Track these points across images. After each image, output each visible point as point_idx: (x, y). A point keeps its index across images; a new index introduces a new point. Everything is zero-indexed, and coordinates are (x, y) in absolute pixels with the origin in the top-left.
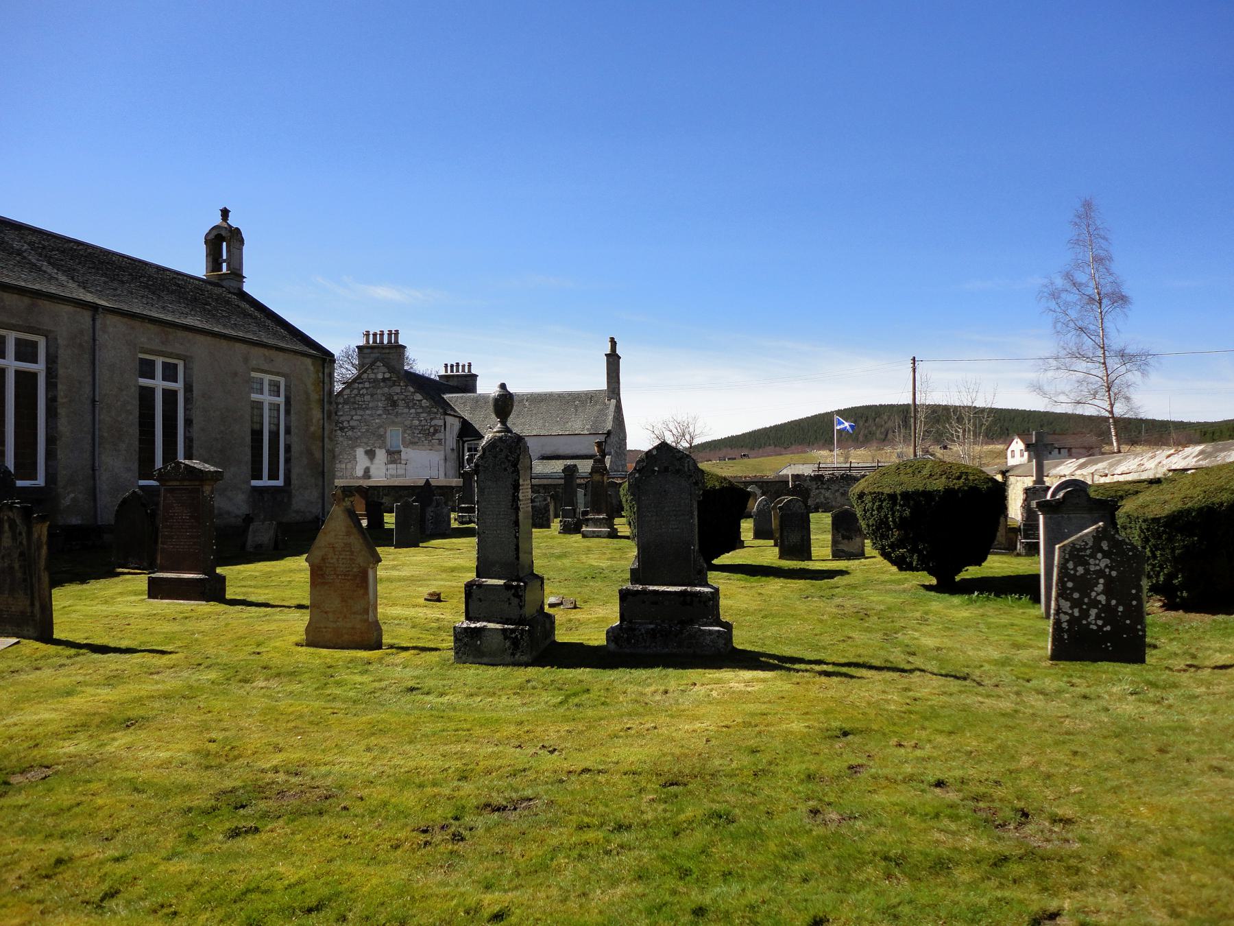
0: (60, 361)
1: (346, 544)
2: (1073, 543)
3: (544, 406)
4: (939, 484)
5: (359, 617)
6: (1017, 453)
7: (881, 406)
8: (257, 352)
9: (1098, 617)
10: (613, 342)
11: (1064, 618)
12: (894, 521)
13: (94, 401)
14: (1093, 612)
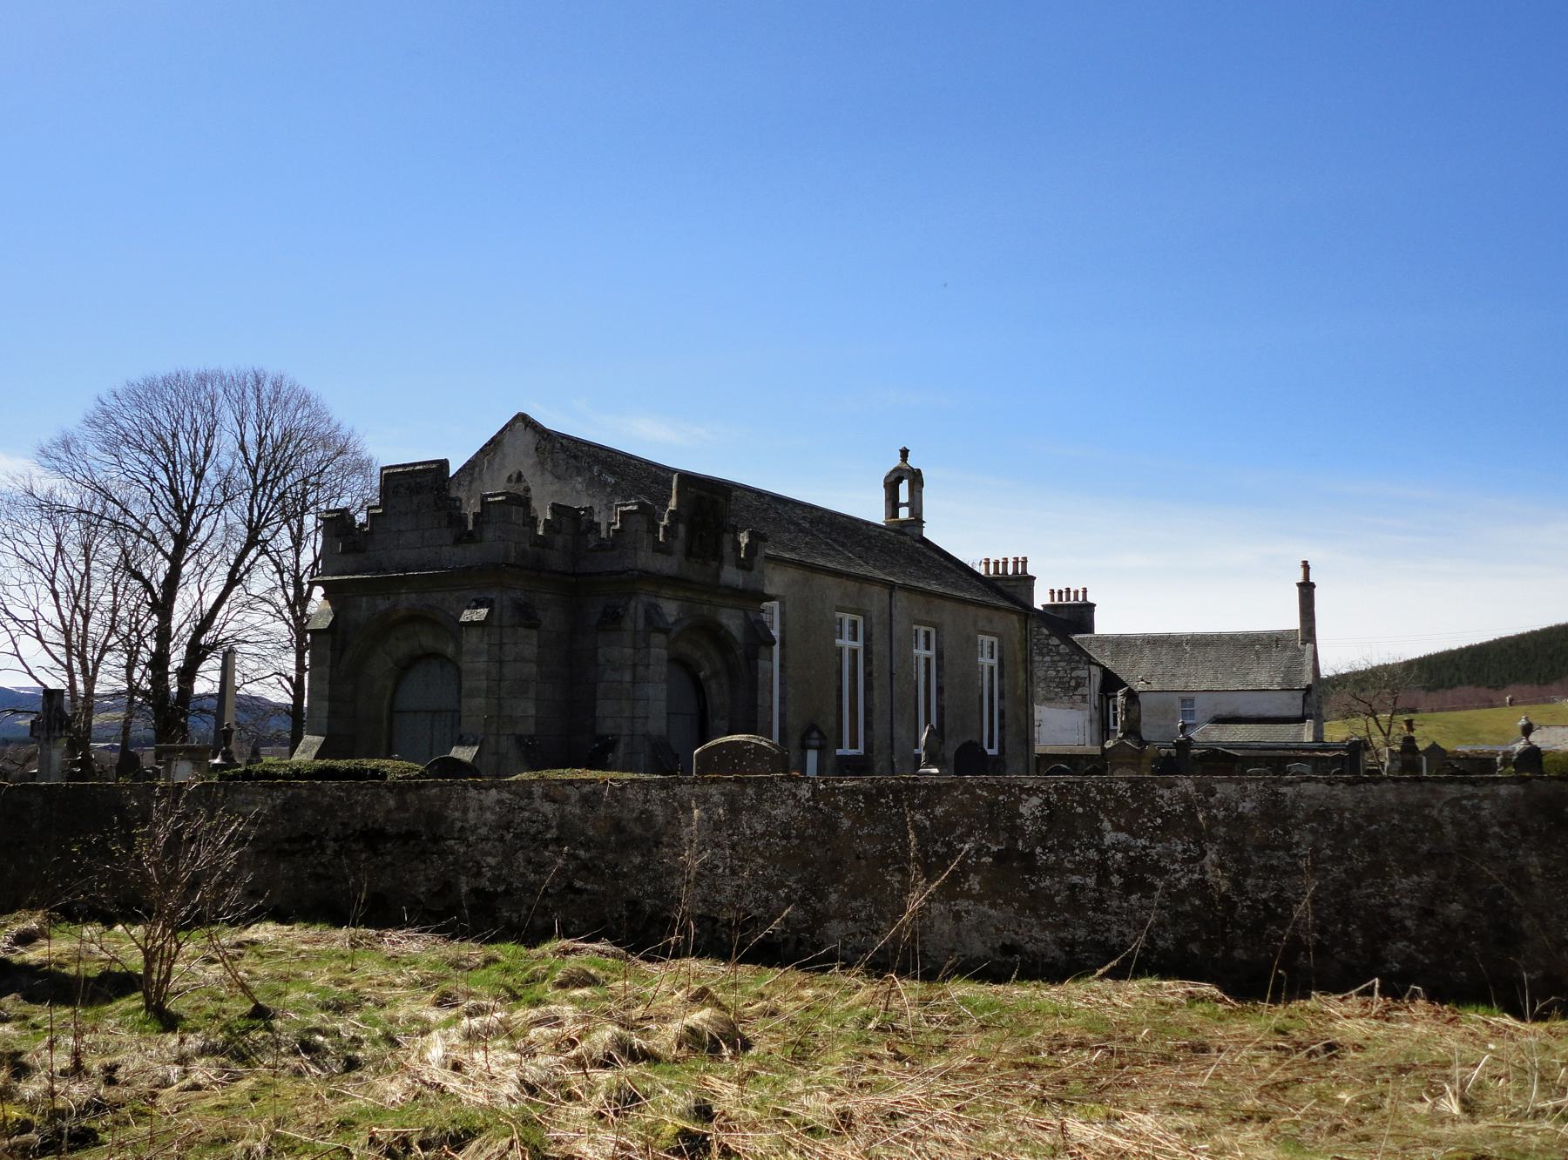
0: (874, 638)
3: (1212, 653)
8: (983, 612)
10: (1306, 566)
13: (892, 674)
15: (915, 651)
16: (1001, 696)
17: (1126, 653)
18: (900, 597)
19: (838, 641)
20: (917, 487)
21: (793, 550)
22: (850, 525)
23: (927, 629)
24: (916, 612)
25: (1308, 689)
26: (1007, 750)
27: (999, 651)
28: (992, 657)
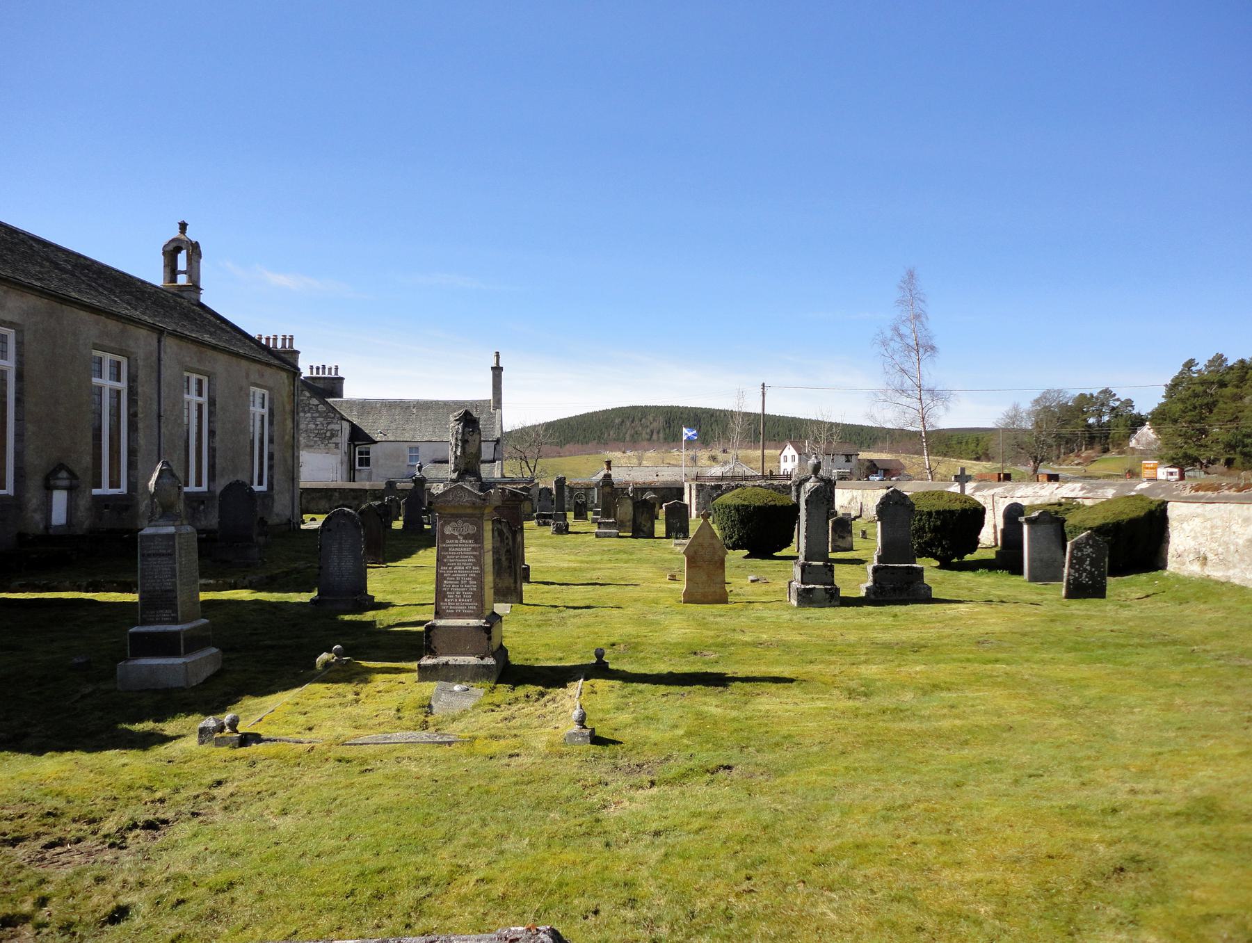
0: (139, 380)
1: (710, 544)
2: (1076, 541)
3: (431, 415)
4: (957, 506)
5: (718, 586)
6: (789, 459)
7: (646, 407)
8: (255, 367)
9: (1086, 577)
10: (497, 355)
11: (1071, 578)
12: (929, 528)
13: (159, 416)
14: (1084, 574)
15: (186, 396)
16: (271, 441)
17: (368, 413)
18: (170, 344)
19: (95, 380)
20: (195, 257)
21: (39, 280)
22: (122, 279)
23: (200, 377)
24: (188, 359)
25: (498, 441)
26: (275, 486)
27: (270, 403)
28: (263, 408)
